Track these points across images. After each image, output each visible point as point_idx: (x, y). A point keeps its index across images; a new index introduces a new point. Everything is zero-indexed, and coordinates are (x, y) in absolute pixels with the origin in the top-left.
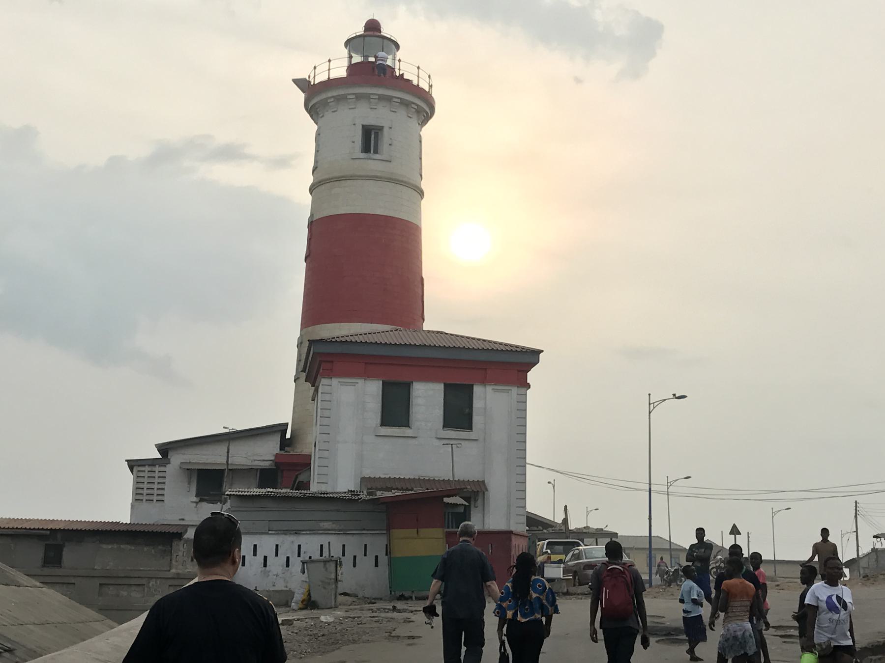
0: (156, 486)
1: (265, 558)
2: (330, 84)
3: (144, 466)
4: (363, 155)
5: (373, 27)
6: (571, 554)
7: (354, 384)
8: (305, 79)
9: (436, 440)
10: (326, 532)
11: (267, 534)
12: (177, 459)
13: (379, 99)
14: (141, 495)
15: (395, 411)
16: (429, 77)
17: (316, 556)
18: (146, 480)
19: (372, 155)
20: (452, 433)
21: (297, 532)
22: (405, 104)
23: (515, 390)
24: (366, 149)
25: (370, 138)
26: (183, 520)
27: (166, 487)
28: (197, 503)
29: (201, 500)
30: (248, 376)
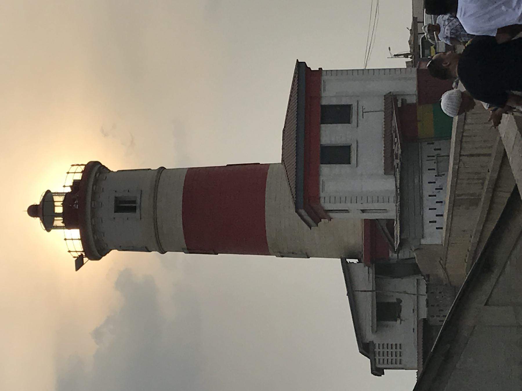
0: (390, 350)
1: (437, 215)
2: (84, 239)
3: (375, 359)
4: (138, 211)
5: (33, 211)
6: (430, 40)
7: (323, 182)
8: (76, 261)
9: (359, 128)
10: (421, 180)
11: (423, 215)
12: (370, 337)
13: (94, 201)
14: (398, 364)
15: (341, 155)
16: (73, 165)
17: (434, 173)
18: (386, 358)
19: (138, 205)
20: (354, 118)
21: (421, 198)
22: (96, 181)
23: (324, 77)
24: (133, 209)
25: (125, 206)
26: (414, 329)
27: (390, 343)
28: (401, 320)
29: (399, 317)
30: (306, 291)
